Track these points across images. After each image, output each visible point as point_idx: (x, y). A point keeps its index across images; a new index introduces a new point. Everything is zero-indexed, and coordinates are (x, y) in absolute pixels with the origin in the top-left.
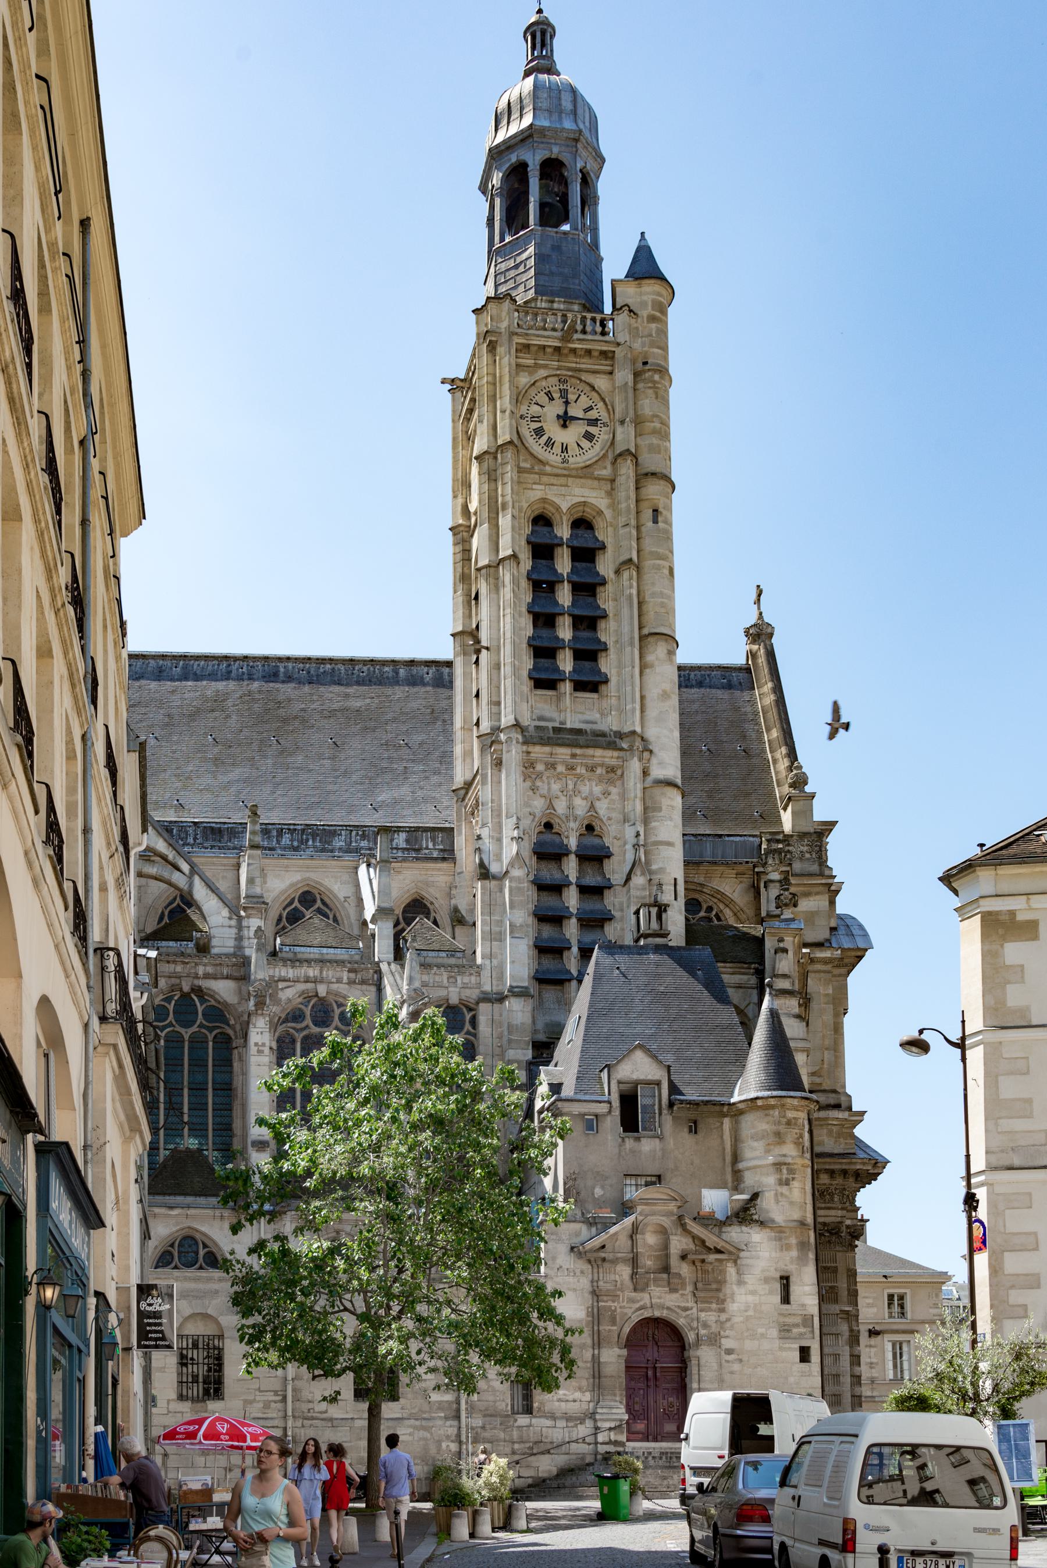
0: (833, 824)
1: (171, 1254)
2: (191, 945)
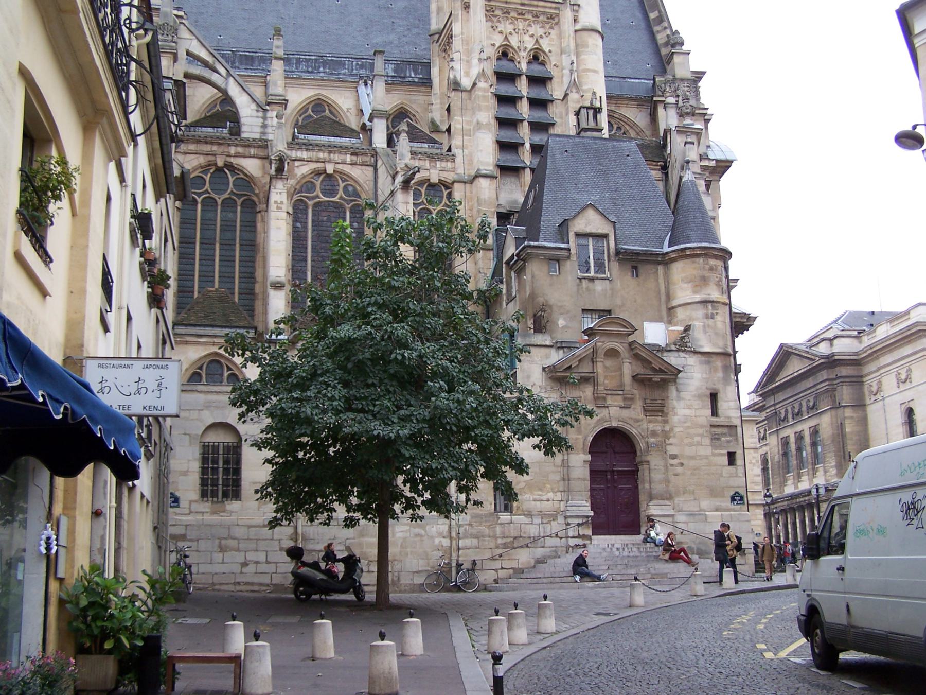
0: (704, 73)
1: (199, 375)
2: (225, 131)
